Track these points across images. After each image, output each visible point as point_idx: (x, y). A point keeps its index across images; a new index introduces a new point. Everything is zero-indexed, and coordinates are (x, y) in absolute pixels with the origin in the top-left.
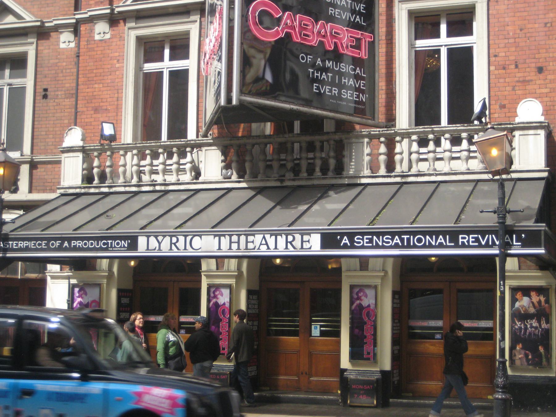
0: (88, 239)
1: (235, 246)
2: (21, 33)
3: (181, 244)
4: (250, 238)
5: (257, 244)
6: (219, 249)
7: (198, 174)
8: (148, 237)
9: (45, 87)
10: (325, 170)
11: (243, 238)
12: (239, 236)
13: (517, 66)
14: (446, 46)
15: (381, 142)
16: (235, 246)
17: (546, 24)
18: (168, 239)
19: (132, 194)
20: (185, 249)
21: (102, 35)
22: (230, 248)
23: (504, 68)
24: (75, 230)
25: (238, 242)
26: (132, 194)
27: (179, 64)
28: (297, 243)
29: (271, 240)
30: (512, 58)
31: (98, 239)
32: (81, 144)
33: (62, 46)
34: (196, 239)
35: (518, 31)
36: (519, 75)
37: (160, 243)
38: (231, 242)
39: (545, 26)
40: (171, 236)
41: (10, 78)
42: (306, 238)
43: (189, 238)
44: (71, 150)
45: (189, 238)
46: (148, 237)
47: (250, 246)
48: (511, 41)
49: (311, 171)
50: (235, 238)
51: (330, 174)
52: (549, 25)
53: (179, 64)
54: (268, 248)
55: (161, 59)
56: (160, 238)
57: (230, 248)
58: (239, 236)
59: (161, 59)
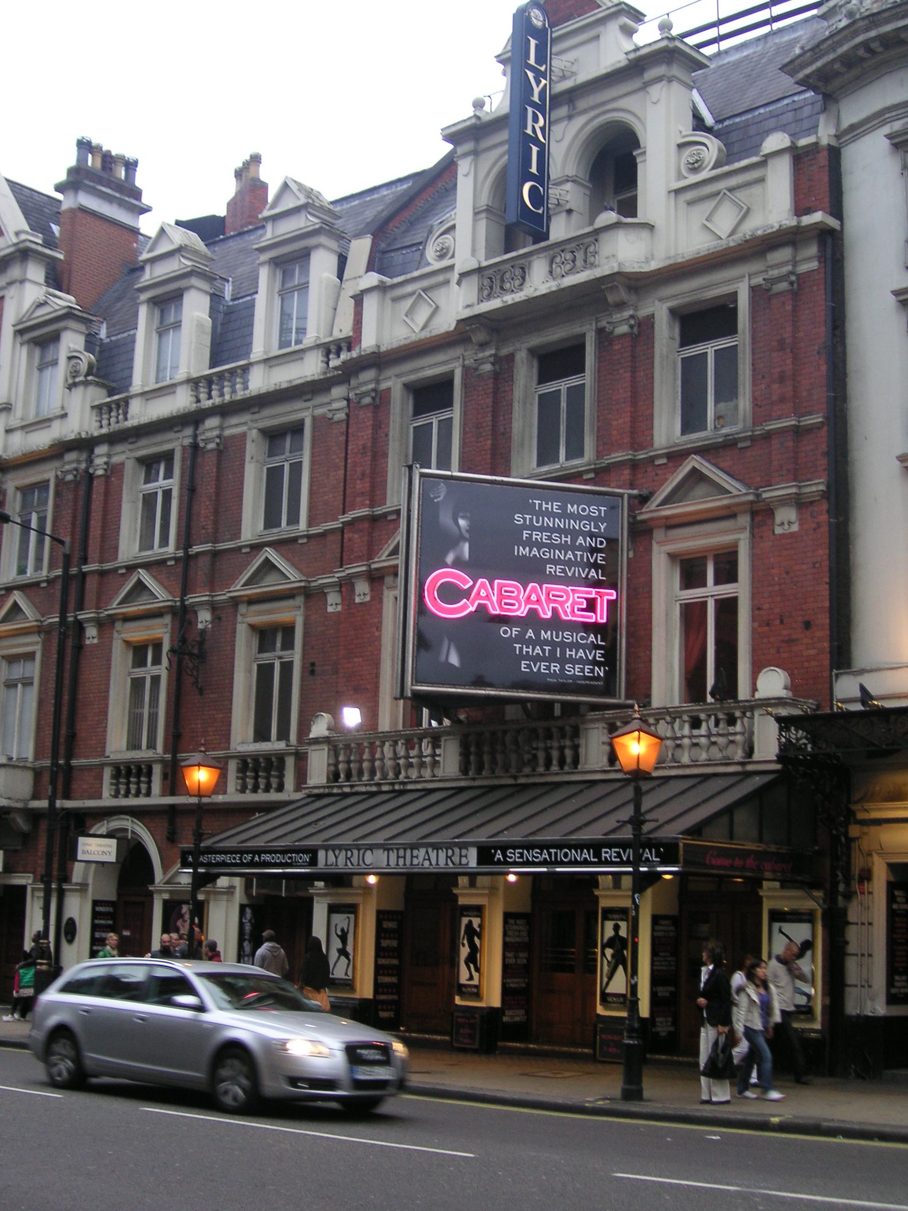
0: (275, 852)
1: (401, 861)
2: (288, 595)
3: (354, 860)
4: (415, 852)
5: (421, 859)
6: (388, 865)
7: (750, 751)
8: (327, 851)
9: (312, 661)
10: (562, 762)
11: (408, 852)
12: (405, 849)
13: (782, 621)
14: (712, 596)
15: (684, 721)
16: (401, 861)
17: (814, 563)
18: (344, 852)
19: (423, 793)
20: (359, 865)
21: (786, 526)
22: (397, 864)
23: (768, 625)
24: (606, 834)
25: (404, 857)
26: (423, 793)
27: (726, 590)
28: (456, 859)
29: (433, 855)
30: (777, 610)
31: (284, 852)
32: (326, 733)
33: (330, 609)
34: (369, 853)
35: (784, 575)
36: (785, 632)
37: (336, 857)
38: (398, 857)
39: (814, 567)
40: (346, 850)
41: (282, 650)
42: (464, 852)
43: (361, 852)
44: (316, 741)
45: (361, 852)
46: (327, 851)
47: (415, 861)
48: (777, 588)
49: (548, 763)
50: (401, 853)
51: (566, 768)
52: (817, 565)
53: (726, 590)
54: (431, 864)
55: (704, 585)
56: (337, 852)
57: (397, 864)
58: (405, 849)
59: (704, 585)
